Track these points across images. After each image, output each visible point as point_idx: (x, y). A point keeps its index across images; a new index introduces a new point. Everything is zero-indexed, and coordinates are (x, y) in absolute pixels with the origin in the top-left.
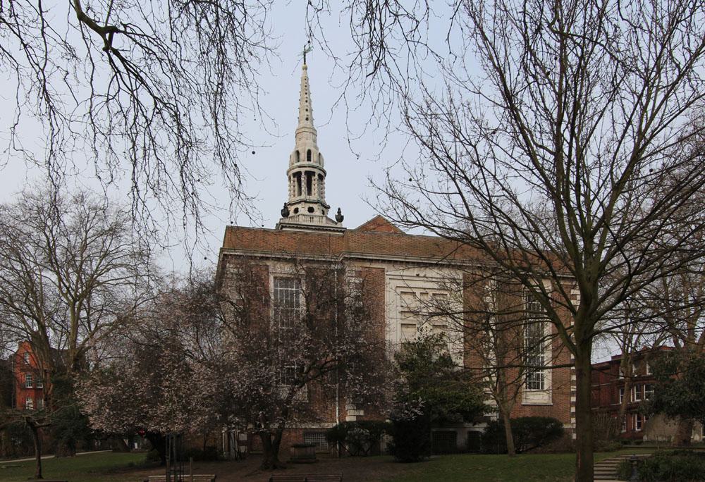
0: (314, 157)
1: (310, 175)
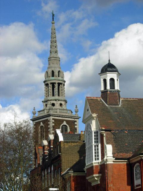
0: (56, 73)
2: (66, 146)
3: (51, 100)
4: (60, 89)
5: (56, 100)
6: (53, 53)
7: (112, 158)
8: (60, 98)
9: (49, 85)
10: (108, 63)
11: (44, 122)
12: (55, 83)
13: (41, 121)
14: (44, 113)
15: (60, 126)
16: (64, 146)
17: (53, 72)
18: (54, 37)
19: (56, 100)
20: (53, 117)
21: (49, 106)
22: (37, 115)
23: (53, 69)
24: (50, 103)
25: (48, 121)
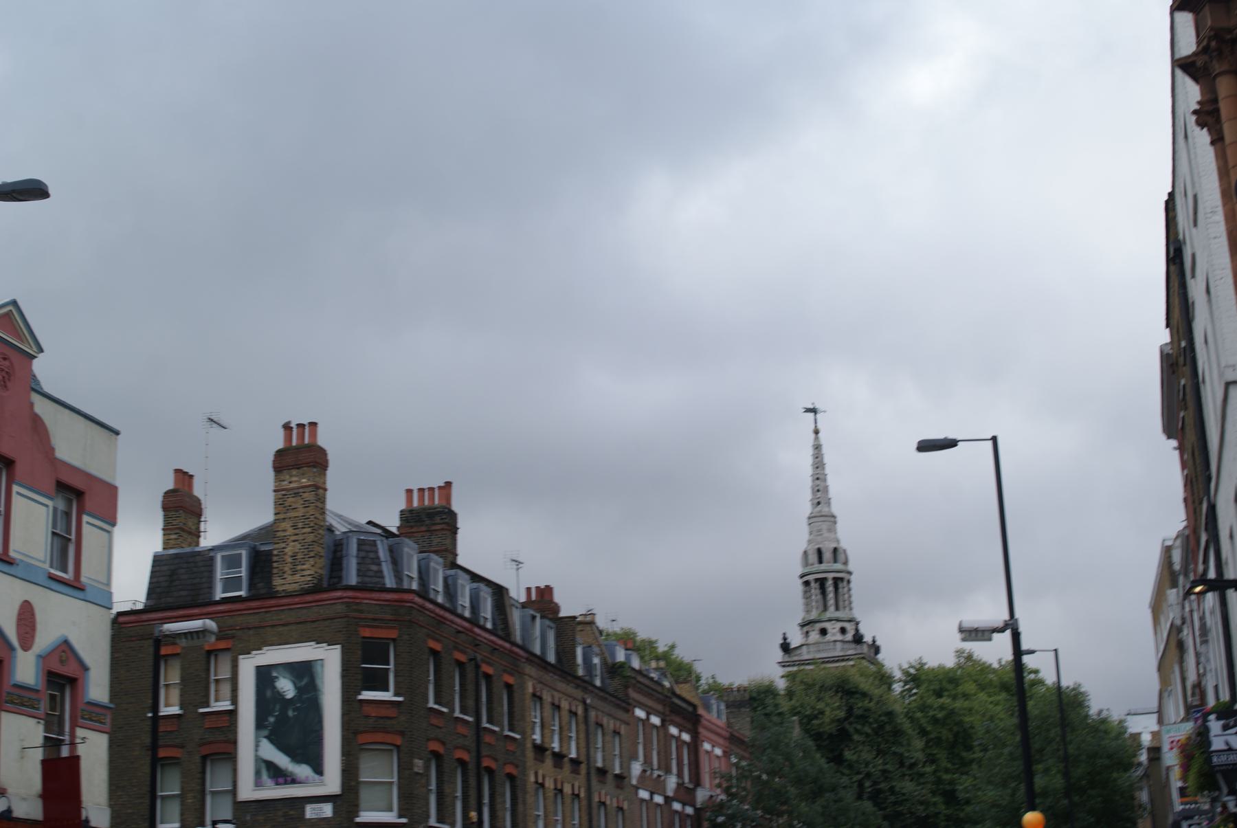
0: (827, 555)
1: (837, 581)
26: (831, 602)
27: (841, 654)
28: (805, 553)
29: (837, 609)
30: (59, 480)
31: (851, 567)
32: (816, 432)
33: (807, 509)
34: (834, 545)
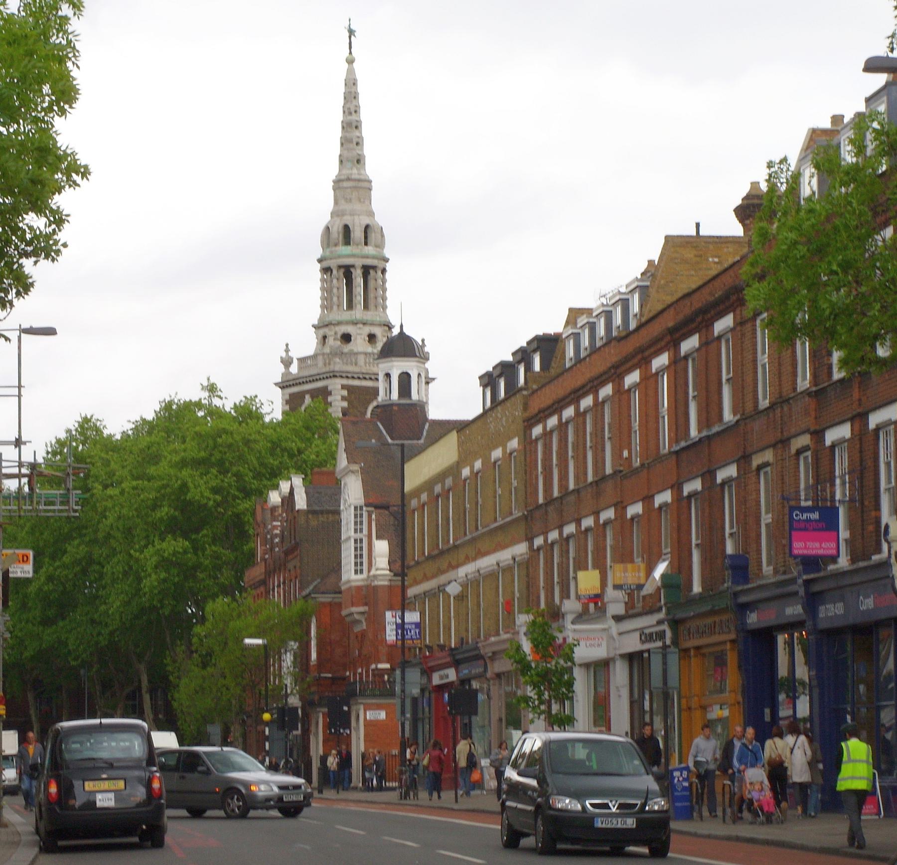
0: (357, 234)
2: (314, 522)
3: (339, 323)
4: (371, 284)
5: (355, 323)
6: (349, 165)
7: (388, 572)
8: (369, 316)
9: (335, 272)
10: (399, 334)
11: (314, 393)
12: (353, 266)
13: (308, 392)
14: (316, 365)
15: (367, 408)
16: (307, 521)
17: (347, 230)
18: (353, 110)
19: (355, 323)
20: (345, 382)
21: (333, 343)
22: (294, 369)
23: (347, 220)
24: (336, 333)
25: (325, 393)
26: (359, 298)
27: (324, 370)
28: (327, 229)
29: (366, 307)
30: (280, 785)
31: (387, 253)
32: (350, 61)
33: (333, 170)
34: (365, 221)
